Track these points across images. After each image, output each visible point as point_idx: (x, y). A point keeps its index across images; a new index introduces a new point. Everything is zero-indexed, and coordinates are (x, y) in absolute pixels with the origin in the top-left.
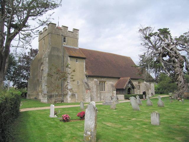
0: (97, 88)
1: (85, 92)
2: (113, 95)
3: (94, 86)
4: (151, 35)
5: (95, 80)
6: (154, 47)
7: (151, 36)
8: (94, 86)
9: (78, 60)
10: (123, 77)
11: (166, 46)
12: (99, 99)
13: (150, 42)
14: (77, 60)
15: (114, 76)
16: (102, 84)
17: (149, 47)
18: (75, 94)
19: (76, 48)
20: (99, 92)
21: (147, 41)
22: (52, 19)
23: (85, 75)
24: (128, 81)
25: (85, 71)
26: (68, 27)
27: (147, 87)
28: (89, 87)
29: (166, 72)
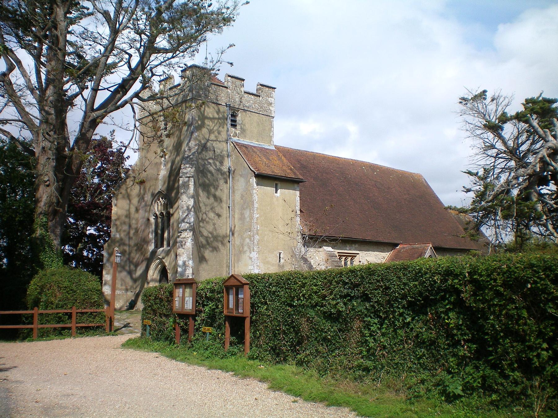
4: (504, 119)
5: (325, 248)
6: (512, 153)
7: (505, 122)
9: (279, 185)
10: (406, 242)
11: (549, 156)
13: (500, 137)
14: (276, 185)
15: (381, 240)
17: (497, 154)
21: (490, 136)
22: (228, 63)
26: (243, 80)
29: (547, 229)
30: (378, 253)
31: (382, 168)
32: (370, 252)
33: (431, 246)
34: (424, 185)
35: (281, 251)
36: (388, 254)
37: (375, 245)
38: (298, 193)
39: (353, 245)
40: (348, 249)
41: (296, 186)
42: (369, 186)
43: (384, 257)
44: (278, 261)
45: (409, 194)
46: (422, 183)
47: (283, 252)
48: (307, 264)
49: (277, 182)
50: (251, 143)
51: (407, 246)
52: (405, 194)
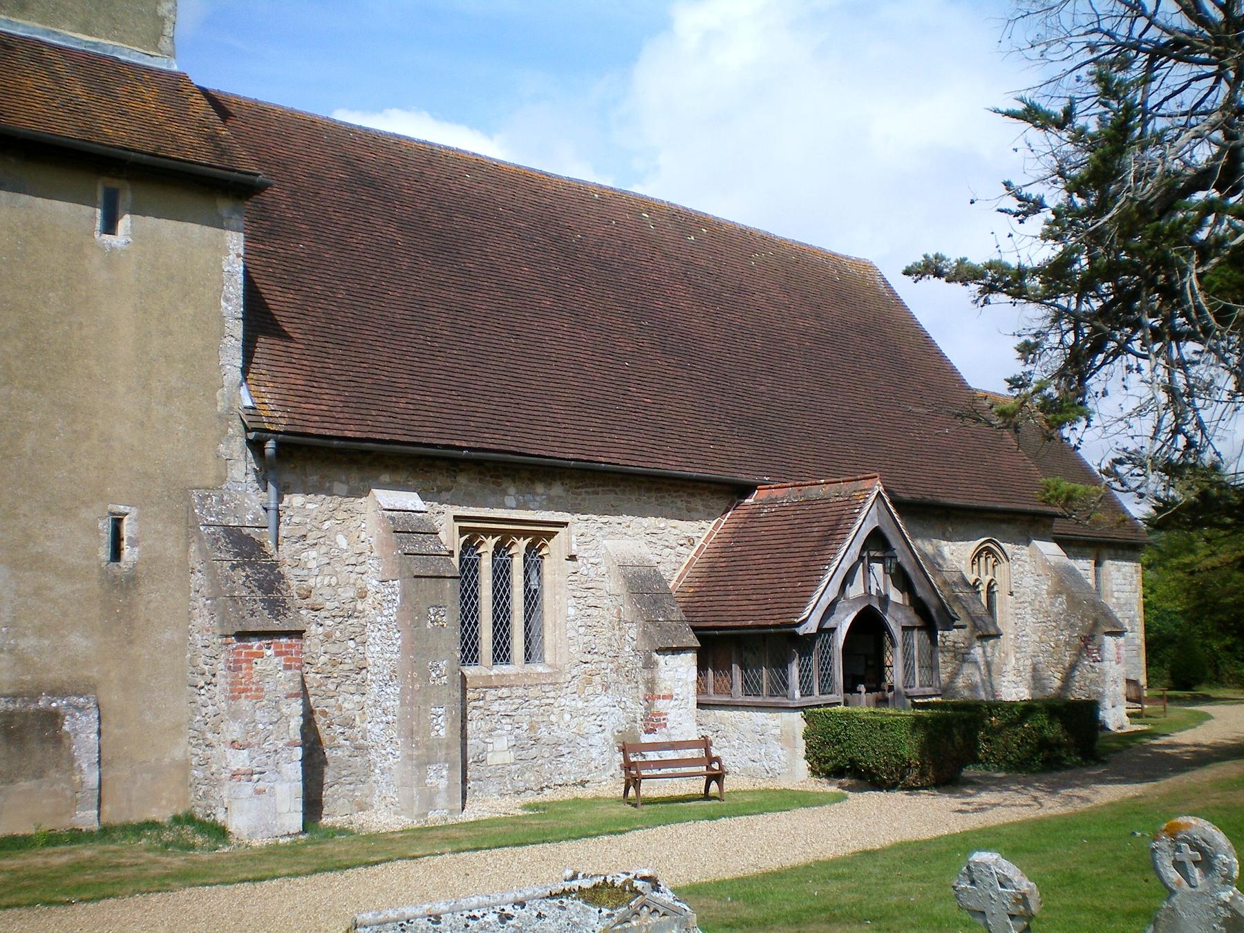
0: (412, 614)
1: (222, 681)
2: (653, 722)
3: (372, 583)
8: (372, 583)
10: (786, 474)
12: (441, 778)
15: (672, 466)
16: (502, 573)
18: (53, 719)
19: (130, 54)
20: (444, 666)
23: (236, 428)
24: (866, 520)
25: (232, 359)
27: (1074, 602)
28: (276, 606)
30: (662, 522)
31: (720, 224)
32: (626, 519)
33: (878, 487)
34: (880, 296)
35: (122, 508)
36: (709, 526)
37: (649, 490)
38: (235, 242)
39: (540, 488)
40: (510, 501)
41: (224, 207)
42: (654, 276)
43: (690, 539)
44: (104, 553)
45: (818, 317)
46: (874, 288)
47: (133, 512)
48: (251, 565)
49: (115, 183)
50: (48, 33)
51: (784, 495)
52: (803, 316)
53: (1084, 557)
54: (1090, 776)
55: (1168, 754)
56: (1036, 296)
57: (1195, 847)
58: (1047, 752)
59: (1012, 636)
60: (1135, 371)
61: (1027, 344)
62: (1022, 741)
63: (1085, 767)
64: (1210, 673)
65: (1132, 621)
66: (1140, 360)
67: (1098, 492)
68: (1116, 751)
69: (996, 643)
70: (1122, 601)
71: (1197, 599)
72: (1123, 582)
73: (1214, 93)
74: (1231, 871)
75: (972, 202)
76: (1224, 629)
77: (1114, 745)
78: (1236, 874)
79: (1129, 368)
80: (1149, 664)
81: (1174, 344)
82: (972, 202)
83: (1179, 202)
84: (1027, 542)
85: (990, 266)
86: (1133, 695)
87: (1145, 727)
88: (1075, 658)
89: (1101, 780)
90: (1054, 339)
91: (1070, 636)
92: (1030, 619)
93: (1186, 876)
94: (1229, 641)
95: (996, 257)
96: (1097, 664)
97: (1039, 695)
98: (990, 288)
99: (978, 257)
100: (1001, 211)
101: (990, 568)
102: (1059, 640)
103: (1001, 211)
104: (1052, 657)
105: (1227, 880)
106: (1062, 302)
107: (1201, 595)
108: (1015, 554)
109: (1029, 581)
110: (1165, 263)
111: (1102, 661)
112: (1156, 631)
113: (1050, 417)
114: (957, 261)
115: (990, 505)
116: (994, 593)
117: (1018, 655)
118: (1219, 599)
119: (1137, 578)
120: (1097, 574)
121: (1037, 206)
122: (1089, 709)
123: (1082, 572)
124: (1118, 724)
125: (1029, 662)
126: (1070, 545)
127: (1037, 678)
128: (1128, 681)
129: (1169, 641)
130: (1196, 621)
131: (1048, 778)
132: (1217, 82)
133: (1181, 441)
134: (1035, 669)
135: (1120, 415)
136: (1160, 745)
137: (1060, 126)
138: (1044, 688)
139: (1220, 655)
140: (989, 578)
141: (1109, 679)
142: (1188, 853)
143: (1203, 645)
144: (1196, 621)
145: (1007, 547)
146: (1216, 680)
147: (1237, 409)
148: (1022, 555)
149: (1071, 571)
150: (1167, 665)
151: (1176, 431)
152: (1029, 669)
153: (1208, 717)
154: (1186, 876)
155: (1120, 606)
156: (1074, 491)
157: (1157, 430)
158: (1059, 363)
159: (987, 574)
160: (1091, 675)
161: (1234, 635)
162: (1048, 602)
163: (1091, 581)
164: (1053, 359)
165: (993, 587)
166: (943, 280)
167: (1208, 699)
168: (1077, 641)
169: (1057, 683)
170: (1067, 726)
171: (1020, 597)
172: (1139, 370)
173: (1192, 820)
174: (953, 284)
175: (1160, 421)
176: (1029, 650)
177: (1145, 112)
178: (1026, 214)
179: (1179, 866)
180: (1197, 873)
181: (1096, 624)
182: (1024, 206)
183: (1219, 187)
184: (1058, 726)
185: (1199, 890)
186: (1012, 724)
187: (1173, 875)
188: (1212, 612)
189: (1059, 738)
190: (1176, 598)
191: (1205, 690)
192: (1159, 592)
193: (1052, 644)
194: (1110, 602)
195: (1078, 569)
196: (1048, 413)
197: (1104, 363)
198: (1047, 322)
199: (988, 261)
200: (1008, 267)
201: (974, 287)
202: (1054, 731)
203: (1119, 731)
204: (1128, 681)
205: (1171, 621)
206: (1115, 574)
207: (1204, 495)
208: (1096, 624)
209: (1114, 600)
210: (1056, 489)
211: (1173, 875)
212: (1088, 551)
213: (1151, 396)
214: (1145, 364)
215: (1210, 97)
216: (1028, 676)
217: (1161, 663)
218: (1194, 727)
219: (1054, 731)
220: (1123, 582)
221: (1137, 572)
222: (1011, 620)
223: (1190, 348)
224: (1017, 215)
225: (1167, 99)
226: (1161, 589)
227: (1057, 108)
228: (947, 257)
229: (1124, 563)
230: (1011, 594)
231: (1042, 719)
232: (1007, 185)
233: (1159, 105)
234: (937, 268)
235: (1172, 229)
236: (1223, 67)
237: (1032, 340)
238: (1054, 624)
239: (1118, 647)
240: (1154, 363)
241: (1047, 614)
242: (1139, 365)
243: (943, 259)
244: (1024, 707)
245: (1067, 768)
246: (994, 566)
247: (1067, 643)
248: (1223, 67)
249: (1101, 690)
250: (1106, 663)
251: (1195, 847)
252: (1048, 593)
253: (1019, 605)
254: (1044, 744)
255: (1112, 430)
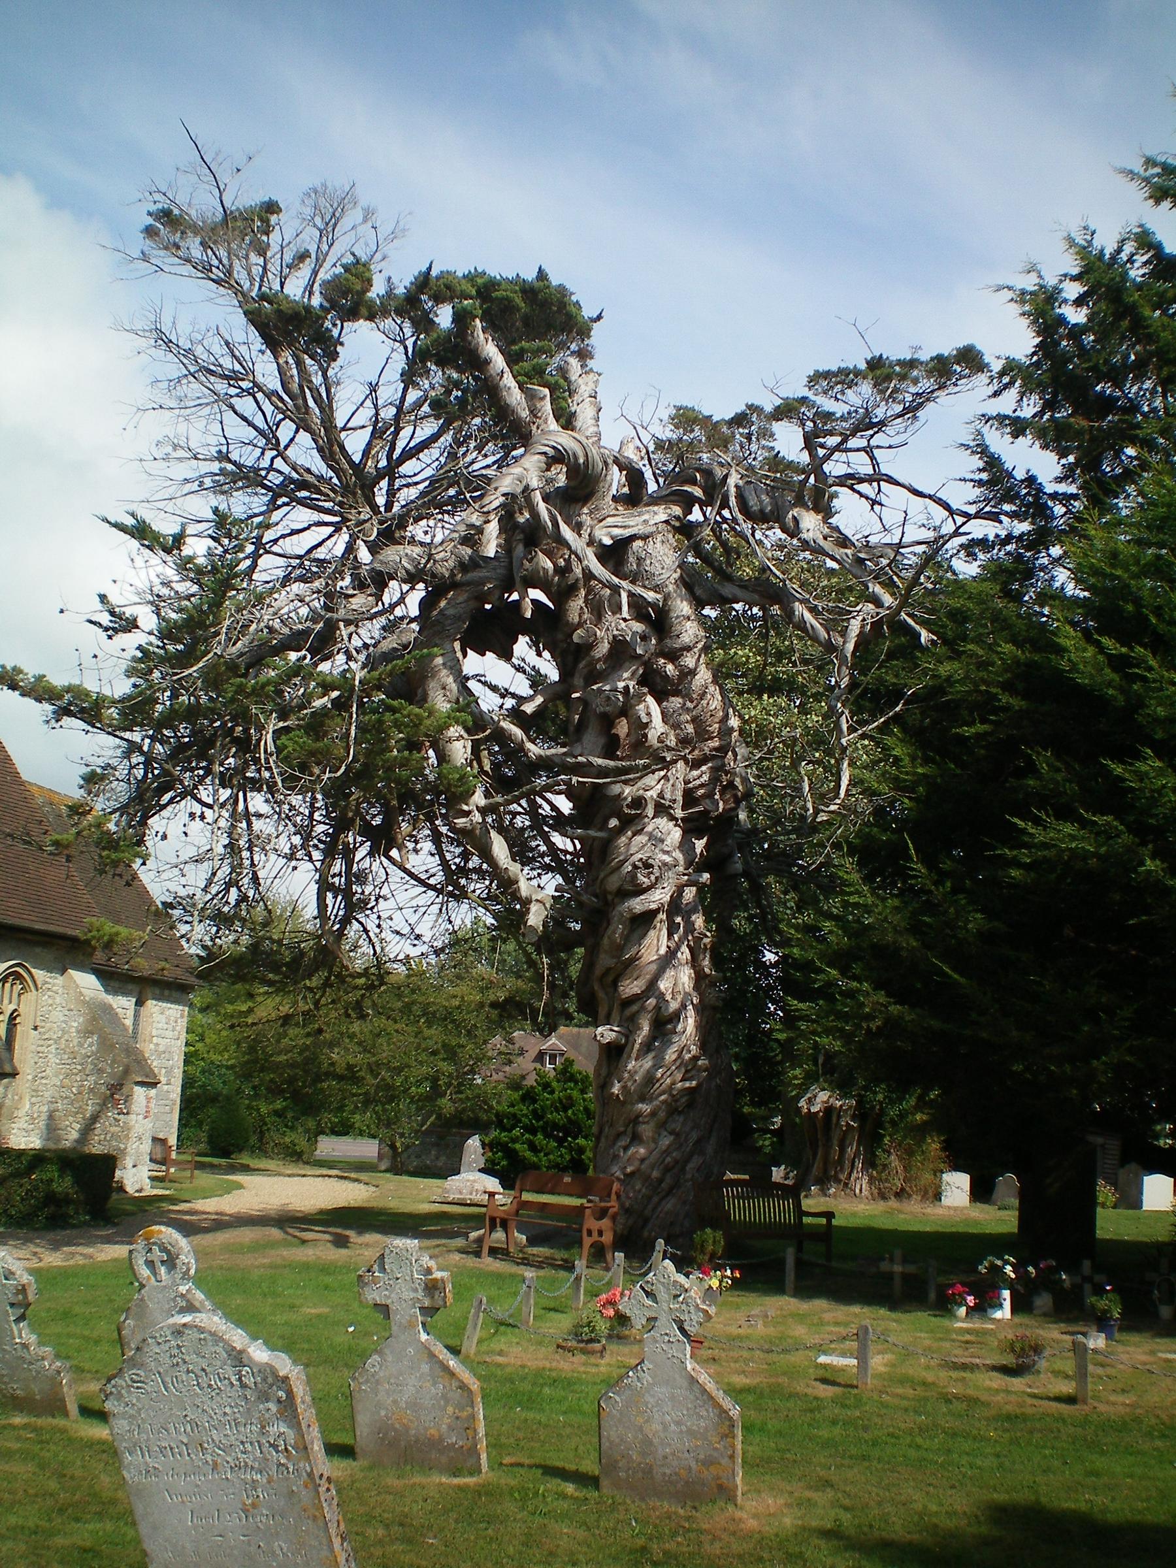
27: (106, 1045)
53: (126, 993)
54: (97, 1236)
55: (186, 1220)
56: (110, 726)
57: (164, 1249)
58: (52, 1208)
59: (30, 1077)
60: (197, 819)
61: (93, 773)
62: (26, 1194)
63: (93, 1226)
64: (253, 1140)
65: (169, 1071)
66: (204, 809)
67: (141, 938)
68: (133, 1214)
69: (10, 1083)
70: (161, 1048)
71: (249, 1054)
72: (166, 1026)
73: (333, 539)
74: (189, 1270)
75: (62, 611)
76: (275, 1091)
77: (128, 1207)
78: (192, 1272)
79: (192, 816)
80: (183, 1124)
81: (241, 794)
82: (62, 611)
83: (268, 659)
84: (63, 971)
85: (69, 689)
86: (159, 1156)
87: (167, 1192)
88: (98, 1108)
89: (109, 1240)
90: (121, 773)
91: (96, 1083)
92: (53, 1060)
93: (155, 1273)
94: (279, 1104)
95: (76, 681)
96: (121, 1116)
97: (52, 1146)
98: (65, 711)
99: (59, 680)
100: (91, 622)
101: (15, 995)
102: (83, 1086)
103: (91, 622)
104: (72, 1104)
105: (185, 1276)
106: (136, 737)
107: (252, 1049)
108: (46, 983)
109: (57, 1015)
110: (243, 716)
111: (128, 1113)
112: (200, 1086)
113: (105, 853)
114: (34, 676)
115: (26, 924)
116: (15, 1025)
117: (34, 1100)
118: (272, 1055)
119: (183, 1024)
120: (137, 1015)
121: (131, 625)
122: (108, 1163)
123: (119, 1010)
124: (137, 1187)
125: (45, 1109)
126: (113, 979)
127: (52, 1127)
128: (155, 1140)
129: (214, 1099)
130: (247, 1076)
131: (51, 1235)
132: (338, 530)
133: (234, 894)
134: (51, 1117)
135: (174, 861)
136: (179, 1212)
137: (168, 551)
138: (58, 1139)
139: (267, 1120)
140: (12, 1007)
141: (133, 1134)
142: (157, 1255)
143: (249, 1107)
144: (247, 1076)
145: (39, 974)
146: (259, 1148)
147: (295, 868)
148: (54, 985)
149: (108, 1009)
150: (206, 1128)
151: (228, 885)
152: (44, 1116)
153: (240, 1186)
154: (155, 1273)
155: (159, 1054)
156: (117, 934)
157: (210, 882)
158: (124, 799)
159: (10, 1002)
160: (113, 1129)
161: (285, 1099)
162: (76, 1041)
163: (129, 1022)
164: (120, 791)
165: (15, 1018)
166: (17, 693)
167: (246, 1169)
168: (103, 1088)
169: (74, 1135)
170: (78, 1181)
171: (44, 1033)
172: (202, 817)
173: (163, 1228)
174: (27, 699)
175: (214, 874)
176: (47, 1094)
177: (258, 543)
178: (116, 630)
179: (150, 1264)
180: (163, 1270)
181: (127, 1072)
182: (115, 622)
183: (313, 651)
184: (68, 1181)
185: (163, 1284)
186: (17, 1174)
187: (145, 1272)
188: (262, 1069)
189: (67, 1194)
190: (226, 1050)
191: (245, 1159)
192: (207, 1040)
193: (74, 1090)
194: (148, 1049)
195: (115, 1006)
196: (104, 849)
197: (171, 802)
198: (119, 752)
199: (66, 684)
200: (87, 694)
201: (48, 708)
202: (64, 1185)
203: (137, 1195)
204: (155, 1140)
205: (220, 1076)
206: (157, 1017)
207: (254, 948)
208: (127, 1072)
209: (152, 1046)
210: (98, 931)
211: (145, 1272)
212: (130, 987)
213: (208, 847)
214: (209, 813)
215: (328, 542)
216: (42, 1124)
217: (200, 1124)
218: (221, 1196)
219: (64, 1185)
220: (166, 1026)
221: (182, 1017)
222: (31, 1059)
223: (258, 802)
224: (106, 629)
225: (283, 536)
226: (211, 1038)
227: (166, 527)
228: (26, 671)
229: (169, 1005)
230: (35, 1028)
231: (52, 1172)
232: (103, 598)
233: (275, 541)
234: (12, 680)
235: (254, 689)
236: (345, 520)
237: (99, 771)
238: (79, 1067)
239: (148, 1099)
240: (217, 815)
241: (73, 1056)
242: (203, 813)
243: (20, 672)
244: (33, 1156)
245: (74, 1227)
246: (19, 995)
247: (91, 1090)
248: (345, 520)
249: (122, 1146)
250: (133, 1117)
251: (164, 1249)
252: (78, 1032)
253: (41, 1042)
254: (51, 1199)
255: (165, 876)
